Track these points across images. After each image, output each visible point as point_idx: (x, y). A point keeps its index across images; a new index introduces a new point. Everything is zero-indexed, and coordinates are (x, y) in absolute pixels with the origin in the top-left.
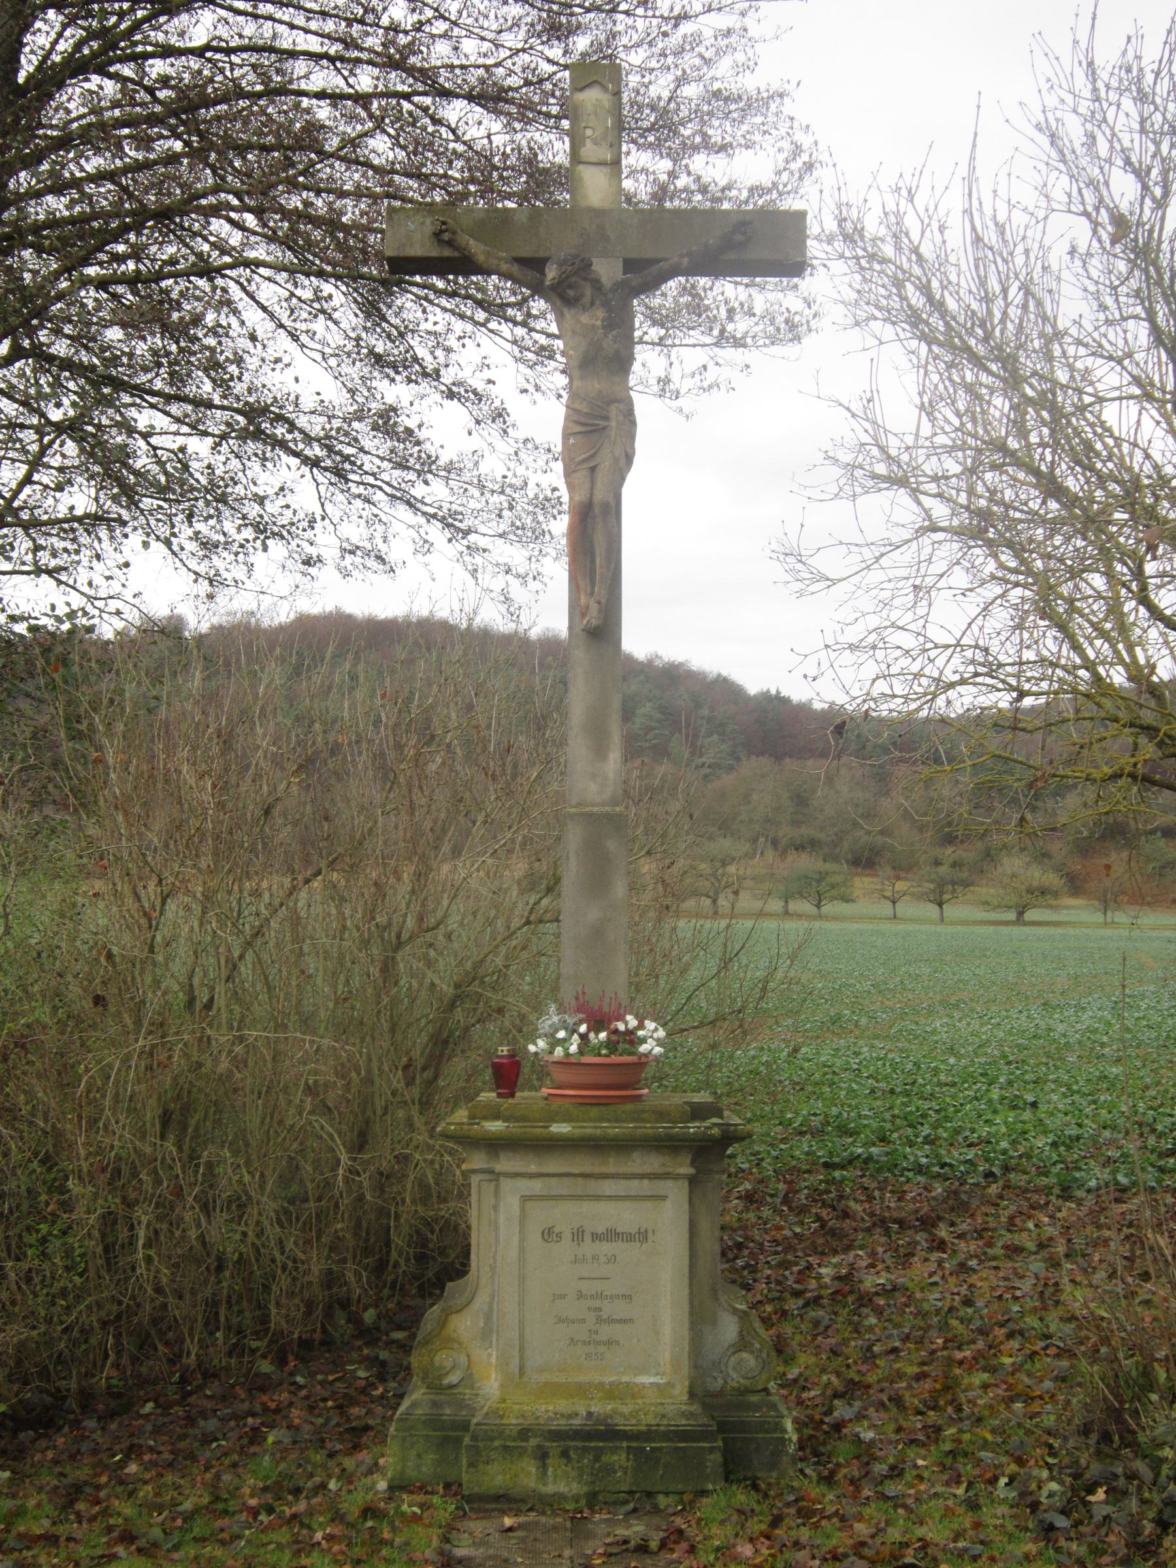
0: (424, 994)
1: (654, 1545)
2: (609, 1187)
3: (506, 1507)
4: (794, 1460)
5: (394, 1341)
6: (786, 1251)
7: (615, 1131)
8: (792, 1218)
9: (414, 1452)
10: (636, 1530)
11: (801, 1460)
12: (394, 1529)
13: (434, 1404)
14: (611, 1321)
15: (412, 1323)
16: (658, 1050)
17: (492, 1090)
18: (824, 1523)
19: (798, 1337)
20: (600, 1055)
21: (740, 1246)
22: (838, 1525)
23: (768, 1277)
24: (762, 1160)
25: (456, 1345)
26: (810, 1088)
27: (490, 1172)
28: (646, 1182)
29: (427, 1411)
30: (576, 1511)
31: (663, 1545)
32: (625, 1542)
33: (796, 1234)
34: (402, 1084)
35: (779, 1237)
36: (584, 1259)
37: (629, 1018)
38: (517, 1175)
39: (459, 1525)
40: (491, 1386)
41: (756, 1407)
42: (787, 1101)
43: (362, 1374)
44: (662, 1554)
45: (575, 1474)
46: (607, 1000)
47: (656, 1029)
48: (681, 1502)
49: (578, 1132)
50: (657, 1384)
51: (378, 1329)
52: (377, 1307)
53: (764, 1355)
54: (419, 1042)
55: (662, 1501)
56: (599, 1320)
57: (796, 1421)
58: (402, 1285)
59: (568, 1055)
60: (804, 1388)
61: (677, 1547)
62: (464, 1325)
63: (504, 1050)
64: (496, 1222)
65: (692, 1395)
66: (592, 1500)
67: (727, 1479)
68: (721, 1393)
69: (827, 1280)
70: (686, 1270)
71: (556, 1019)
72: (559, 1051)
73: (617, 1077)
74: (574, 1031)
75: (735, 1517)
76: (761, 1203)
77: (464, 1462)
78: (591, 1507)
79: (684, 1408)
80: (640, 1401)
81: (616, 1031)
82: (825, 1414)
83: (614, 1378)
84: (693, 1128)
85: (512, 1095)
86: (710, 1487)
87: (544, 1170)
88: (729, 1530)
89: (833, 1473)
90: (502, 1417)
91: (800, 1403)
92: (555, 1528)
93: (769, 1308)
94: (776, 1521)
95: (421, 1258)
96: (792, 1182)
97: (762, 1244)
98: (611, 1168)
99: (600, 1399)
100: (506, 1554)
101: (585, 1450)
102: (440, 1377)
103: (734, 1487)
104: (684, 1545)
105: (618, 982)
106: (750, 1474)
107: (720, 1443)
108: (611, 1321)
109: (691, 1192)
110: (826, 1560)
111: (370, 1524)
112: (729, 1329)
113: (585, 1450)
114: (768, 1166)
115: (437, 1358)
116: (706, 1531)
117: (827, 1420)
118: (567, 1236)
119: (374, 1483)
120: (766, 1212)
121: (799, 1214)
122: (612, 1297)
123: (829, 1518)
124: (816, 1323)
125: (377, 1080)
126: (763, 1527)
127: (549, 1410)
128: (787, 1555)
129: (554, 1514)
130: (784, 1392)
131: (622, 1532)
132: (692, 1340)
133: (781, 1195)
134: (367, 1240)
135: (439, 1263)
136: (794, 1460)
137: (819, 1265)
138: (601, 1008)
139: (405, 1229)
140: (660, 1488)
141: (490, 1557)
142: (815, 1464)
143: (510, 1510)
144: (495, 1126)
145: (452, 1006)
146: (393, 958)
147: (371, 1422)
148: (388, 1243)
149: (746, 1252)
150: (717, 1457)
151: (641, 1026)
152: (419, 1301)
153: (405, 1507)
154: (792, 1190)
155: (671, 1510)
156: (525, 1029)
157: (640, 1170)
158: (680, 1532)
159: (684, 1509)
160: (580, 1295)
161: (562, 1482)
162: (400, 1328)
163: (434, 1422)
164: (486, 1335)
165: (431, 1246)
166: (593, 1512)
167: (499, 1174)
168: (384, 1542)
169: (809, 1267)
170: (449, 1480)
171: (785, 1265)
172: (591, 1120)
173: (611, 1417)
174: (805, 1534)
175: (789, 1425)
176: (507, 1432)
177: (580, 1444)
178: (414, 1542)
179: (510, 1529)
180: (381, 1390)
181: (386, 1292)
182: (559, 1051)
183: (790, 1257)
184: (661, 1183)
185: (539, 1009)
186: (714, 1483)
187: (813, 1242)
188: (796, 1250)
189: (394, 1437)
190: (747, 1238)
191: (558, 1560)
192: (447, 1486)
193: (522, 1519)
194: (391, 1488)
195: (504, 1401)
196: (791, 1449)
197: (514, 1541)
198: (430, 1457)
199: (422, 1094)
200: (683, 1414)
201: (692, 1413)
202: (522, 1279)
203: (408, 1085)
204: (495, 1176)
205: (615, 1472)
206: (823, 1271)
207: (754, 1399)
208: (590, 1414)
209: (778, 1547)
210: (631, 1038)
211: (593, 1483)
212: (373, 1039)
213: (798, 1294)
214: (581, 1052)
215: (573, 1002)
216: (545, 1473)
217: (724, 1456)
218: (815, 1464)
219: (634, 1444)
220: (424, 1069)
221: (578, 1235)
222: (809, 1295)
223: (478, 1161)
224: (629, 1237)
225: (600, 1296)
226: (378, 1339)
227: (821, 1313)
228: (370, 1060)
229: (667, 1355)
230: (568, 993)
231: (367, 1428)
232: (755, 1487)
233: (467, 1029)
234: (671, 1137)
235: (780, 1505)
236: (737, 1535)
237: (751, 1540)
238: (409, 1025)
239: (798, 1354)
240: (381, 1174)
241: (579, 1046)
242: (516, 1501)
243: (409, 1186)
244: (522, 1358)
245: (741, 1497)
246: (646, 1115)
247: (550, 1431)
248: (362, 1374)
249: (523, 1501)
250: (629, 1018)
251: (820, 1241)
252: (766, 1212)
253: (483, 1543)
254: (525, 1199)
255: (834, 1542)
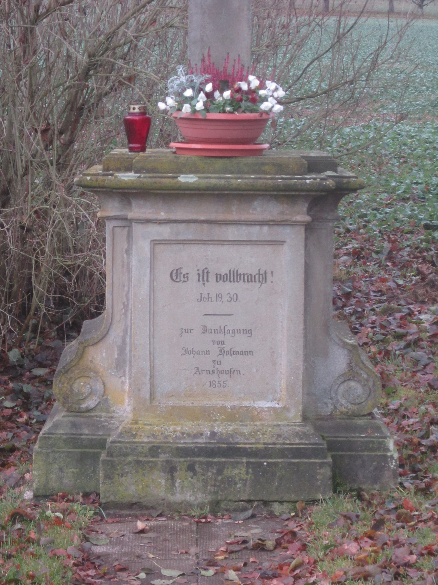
0: (60, 64)
1: (270, 544)
2: (232, 233)
3: (138, 513)
4: (395, 475)
5: (35, 377)
6: (389, 300)
7: (237, 181)
8: (396, 272)
9: (56, 466)
10: (254, 532)
11: (401, 475)
12: (40, 531)
13: (74, 425)
14: (232, 352)
15: (51, 360)
16: (278, 108)
17: (123, 146)
18: (420, 525)
19: (399, 374)
20: (224, 112)
21: (348, 296)
22: (433, 527)
23: (373, 322)
24: (368, 222)
25: (92, 374)
26: (412, 161)
27: (124, 219)
28: (265, 229)
29: (68, 431)
30: (200, 517)
31: (278, 544)
32: (245, 542)
33: (399, 286)
34: (42, 146)
35: (383, 288)
36: (209, 297)
37: (251, 78)
38: (148, 221)
39: (97, 528)
40: (124, 410)
41: (363, 429)
42: (392, 172)
43: (8, 404)
44: (277, 551)
45: (200, 485)
46: (231, 62)
47: (276, 89)
48: (295, 509)
49: (204, 182)
50: (274, 408)
51: (22, 366)
52: (20, 347)
53: (371, 384)
54: (56, 107)
55: (277, 508)
56: (222, 352)
57: (397, 444)
58: (43, 329)
59: (194, 111)
60: (404, 417)
61: (290, 546)
62: (100, 356)
63: (136, 108)
64: (128, 264)
65: (305, 418)
66: (215, 507)
67: (335, 491)
68: (331, 417)
69: (426, 325)
70: (302, 308)
71: (183, 79)
72: (187, 108)
73: (238, 133)
74: (201, 90)
75: (342, 521)
76: (367, 259)
77: (101, 474)
78: (214, 513)
79: (298, 429)
80: (258, 423)
81: (239, 90)
82: (423, 438)
83: (236, 403)
84: (310, 179)
85: (143, 149)
86: (320, 497)
87: (173, 217)
88: (337, 532)
89: (429, 486)
90: (135, 436)
91: (401, 429)
92: (182, 531)
93: (374, 349)
94: (379, 524)
95: (61, 303)
96: (396, 241)
97: (368, 294)
98: (234, 217)
99: (223, 421)
100: (138, 551)
101: (209, 465)
102: (79, 402)
103: (342, 497)
104: (297, 544)
105: (242, 46)
106: (355, 486)
107: (330, 460)
108: (232, 352)
109: (306, 238)
110: (422, 555)
111: (18, 526)
112: (339, 361)
113: (209, 465)
114: (374, 227)
115: (76, 386)
116: (316, 533)
117: (424, 442)
118: (193, 277)
119: (21, 493)
120: (372, 267)
121: (401, 269)
122: (234, 332)
123: (425, 522)
124: (416, 362)
125: (18, 142)
126: (366, 529)
127: (177, 430)
128: (388, 551)
129: (182, 519)
130: (387, 420)
131: (242, 534)
132: (306, 370)
133: (386, 252)
134: (11, 287)
135: (77, 304)
136: (395, 475)
137: (420, 312)
138: (225, 69)
139: (45, 277)
140: (275, 498)
141: (126, 554)
142: (413, 478)
143: (142, 515)
144: (127, 177)
145: (86, 76)
146: (32, 30)
147: (17, 444)
148: (30, 291)
149: (354, 301)
150: (327, 472)
151: (262, 86)
152: (58, 343)
153: (49, 513)
154: (396, 248)
155: (285, 516)
156: (154, 91)
157: (260, 217)
158: (294, 534)
159: (297, 516)
160: (205, 330)
161: (189, 492)
162: (41, 365)
163: (73, 441)
164: (119, 365)
165: (69, 292)
166: (216, 517)
167: (131, 220)
168: (29, 541)
169: (411, 314)
170: (87, 490)
171: (388, 312)
172: (215, 172)
173: (232, 436)
174: (404, 535)
175: (391, 445)
176: (140, 449)
177: (204, 459)
178: (58, 541)
179: (142, 531)
180: (25, 417)
181: (28, 334)
182: (187, 108)
183: (394, 305)
184: (280, 229)
185: (166, 72)
186: (323, 493)
187: (415, 293)
188: (398, 299)
189: (38, 453)
190: (354, 288)
191: (185, 556)
192: (86, 495)
193: (153, 523)
194: (36, 497)
195: (136, 423)
196: (393, 465)
197: (146, 541)
198: (71, 471)
199: (60, 156)
200: (297, 435)
201: (304, 433)
202: (152, 315)
203: (46, 148)
204: (127, 222)
205: (236, 484)
206: (423, 317)
207: (361, 422)
208: (213, 434)
209: (380, 545)
210: (253, 97)
211: (216, 493)
212: (14, 105)
213: (400, 337)
214: (207, 109)
215: (199, 64)
216: (173, 485)
217: (333, 471)
218: (413, 478)
219: (253, 460)
220: (61, 133)
221: (204, 276)
222: (409, 338)
223: (112, 208)
224: (250, 278)
225: (223, 330)
226: (22, 375)
227: (420, 353)
228: (11, 124)
229: (283, 383)
230: (195, 55)
231: (13, 449)
232: (360, 497)
233: (100, 98)
234: (288, 188)
235: (382, 512)
236: (343, 536)
237: (356, 539)
238: (48, 92)
239: (399, 388)
240: (22, 227)
241: (205, 104)
242: (147, 508)
243: (48, 239)
244: (152, 385)
245: (348, 505)
246: (266, 168)
247: (178, 449)
248: (8, 404)
249: (152, 508)
250: (251, 78)
251: (421, 291)
252: (372, 267)
253: (118, 542)
254: (155, 243)
255: (429, 541)
